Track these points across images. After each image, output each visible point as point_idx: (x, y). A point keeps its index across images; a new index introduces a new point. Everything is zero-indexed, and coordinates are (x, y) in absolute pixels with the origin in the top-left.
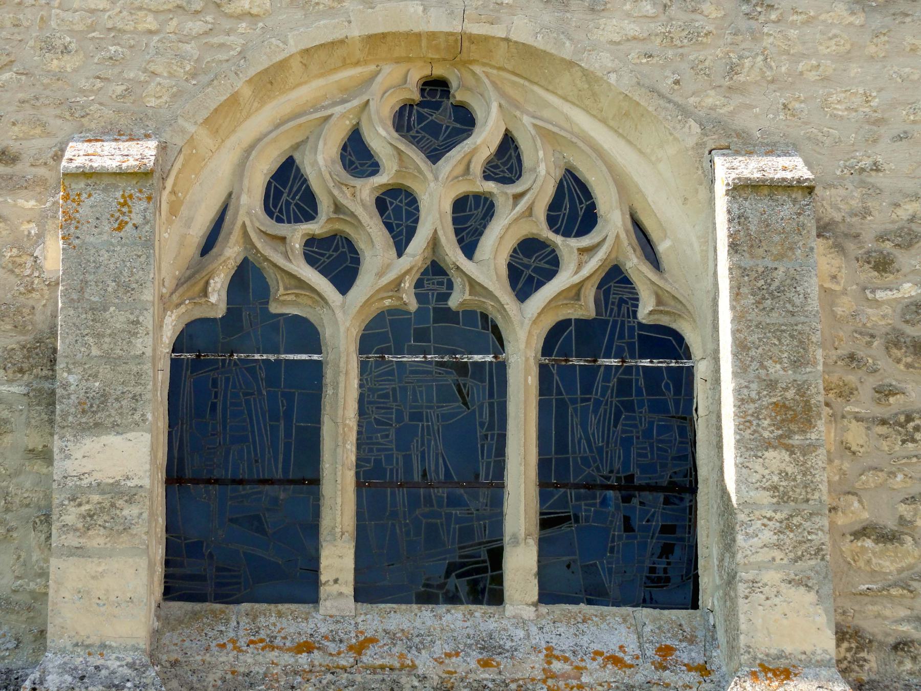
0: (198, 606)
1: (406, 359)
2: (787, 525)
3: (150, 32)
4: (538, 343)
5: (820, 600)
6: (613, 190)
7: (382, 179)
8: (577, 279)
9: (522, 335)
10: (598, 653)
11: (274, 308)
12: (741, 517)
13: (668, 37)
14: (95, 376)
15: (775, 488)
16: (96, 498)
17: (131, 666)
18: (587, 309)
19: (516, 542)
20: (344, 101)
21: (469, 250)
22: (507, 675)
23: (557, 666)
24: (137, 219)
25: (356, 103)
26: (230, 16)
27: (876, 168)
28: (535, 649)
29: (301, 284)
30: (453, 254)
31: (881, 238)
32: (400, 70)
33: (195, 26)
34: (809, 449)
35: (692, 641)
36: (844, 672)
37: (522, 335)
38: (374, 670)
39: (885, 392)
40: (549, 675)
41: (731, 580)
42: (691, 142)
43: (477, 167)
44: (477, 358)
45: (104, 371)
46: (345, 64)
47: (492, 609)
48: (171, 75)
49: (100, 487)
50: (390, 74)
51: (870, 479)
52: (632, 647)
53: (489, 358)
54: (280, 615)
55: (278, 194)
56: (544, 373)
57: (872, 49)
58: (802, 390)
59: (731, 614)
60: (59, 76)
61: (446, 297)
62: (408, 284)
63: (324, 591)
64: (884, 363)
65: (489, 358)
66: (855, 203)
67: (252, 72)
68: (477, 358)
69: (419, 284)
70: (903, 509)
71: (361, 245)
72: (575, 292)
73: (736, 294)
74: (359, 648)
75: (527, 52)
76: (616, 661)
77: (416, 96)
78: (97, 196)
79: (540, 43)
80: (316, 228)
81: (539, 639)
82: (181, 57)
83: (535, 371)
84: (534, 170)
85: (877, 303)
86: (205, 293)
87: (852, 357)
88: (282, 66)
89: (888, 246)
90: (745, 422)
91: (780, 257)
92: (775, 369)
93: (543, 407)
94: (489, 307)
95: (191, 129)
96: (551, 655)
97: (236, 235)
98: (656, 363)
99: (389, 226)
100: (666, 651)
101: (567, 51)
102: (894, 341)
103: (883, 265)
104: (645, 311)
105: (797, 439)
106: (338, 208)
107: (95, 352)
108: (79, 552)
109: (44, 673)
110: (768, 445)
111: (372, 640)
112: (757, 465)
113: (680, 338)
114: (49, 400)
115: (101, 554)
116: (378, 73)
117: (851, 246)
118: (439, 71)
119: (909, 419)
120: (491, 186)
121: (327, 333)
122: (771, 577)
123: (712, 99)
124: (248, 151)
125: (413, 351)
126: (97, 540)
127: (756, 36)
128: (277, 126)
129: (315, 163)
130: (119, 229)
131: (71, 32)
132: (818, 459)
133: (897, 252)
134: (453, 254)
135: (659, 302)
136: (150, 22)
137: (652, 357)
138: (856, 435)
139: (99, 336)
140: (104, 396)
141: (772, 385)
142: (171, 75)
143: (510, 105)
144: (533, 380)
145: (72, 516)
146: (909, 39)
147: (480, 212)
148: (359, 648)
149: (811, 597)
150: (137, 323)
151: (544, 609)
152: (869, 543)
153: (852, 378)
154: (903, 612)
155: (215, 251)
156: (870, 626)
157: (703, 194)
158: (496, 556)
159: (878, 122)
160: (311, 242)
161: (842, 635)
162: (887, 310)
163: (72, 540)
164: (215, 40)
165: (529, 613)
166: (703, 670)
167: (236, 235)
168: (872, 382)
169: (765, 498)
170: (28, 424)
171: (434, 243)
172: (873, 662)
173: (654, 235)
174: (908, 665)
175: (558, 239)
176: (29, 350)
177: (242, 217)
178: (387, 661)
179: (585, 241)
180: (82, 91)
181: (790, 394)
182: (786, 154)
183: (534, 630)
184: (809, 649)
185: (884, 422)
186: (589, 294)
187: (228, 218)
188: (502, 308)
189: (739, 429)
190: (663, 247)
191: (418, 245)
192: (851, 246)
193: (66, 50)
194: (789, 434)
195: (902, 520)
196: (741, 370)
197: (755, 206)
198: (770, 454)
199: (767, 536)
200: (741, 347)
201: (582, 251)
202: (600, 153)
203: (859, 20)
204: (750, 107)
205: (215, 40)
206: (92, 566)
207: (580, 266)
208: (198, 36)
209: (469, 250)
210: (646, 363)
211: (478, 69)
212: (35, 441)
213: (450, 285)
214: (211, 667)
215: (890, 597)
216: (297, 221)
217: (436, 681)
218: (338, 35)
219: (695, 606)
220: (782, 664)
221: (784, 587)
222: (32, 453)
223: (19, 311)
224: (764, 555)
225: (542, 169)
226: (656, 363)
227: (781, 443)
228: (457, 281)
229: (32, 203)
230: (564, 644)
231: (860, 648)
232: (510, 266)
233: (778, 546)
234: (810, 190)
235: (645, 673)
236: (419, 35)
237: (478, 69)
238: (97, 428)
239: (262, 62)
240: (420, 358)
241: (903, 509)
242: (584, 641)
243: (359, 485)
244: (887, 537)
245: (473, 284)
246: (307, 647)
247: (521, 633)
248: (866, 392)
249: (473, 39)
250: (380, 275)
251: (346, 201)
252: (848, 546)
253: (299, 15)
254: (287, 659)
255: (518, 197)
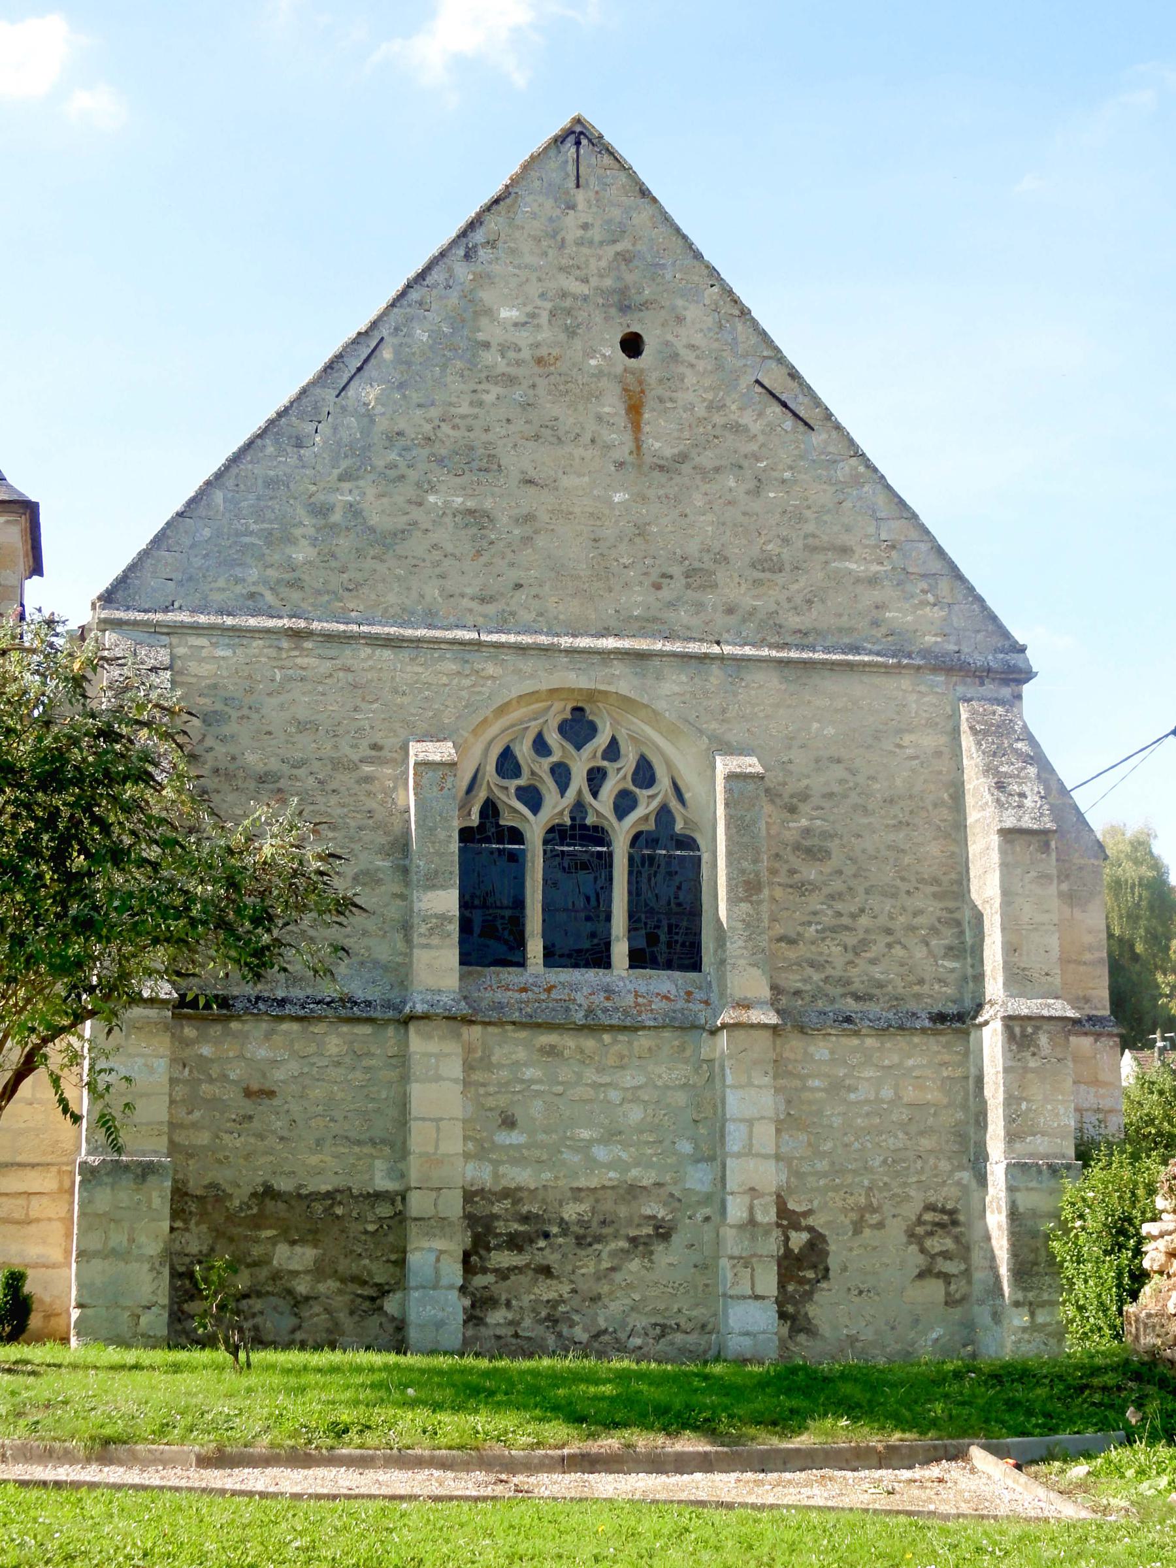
0: (470, 968)
1: (566, 849)
2: (749, 939)
3: (445, 685)
4: (628, 843)
5: (764, 973)
6: (664, 767)
7: (554, 759)
8: (647, 811)
9: (621, 838)
10: (658, 994)
11: (502, 822)
12: (729, 934)
13: (693, 694)
14: (432, 862)
15: (744, 921)
16: (434, 921)
17: (453, 1000)
18: (651, 826)
19: (618, 939)
20: (535, 719)
21: (595, 794)
22: (618, 1005)
23: (640, 1000)
24: (449, 785)
25: (541, 721)
26: (483, 677)
27: (790, 762)
28: (629, 991)
29: (515, 811)
30: (588, 797)
31: (792, 796)
32: (562, 703)
33: (466, 682)
34: (760, 902)
35: (700, 988)
36: (772, 1004)
37: (621, 838)
38: (557, 1001)
39: (792, 872)
40: (637, 1004)
41: (723, 962)
42: (704, 747)
43: (599, 754)
44: (599, 849)
45: (436, 859)
46: (537, 701)
47: (606, 971)
48: (455, 707)
49: (436, 916)
50: (558, 706)
51: (785, 914)
52: (674, 992)
53: (605, 849)
54: (509, 973)
55: (503, 765)
56: (631, 859)
57: (789, 702)
58: (757, 874)
59: (722, 979)
60: (401, 707)
61: (584, 818)
62: (566, 812)
63: (529, 962)
64: (792, 858)
65: (605, 849)
66: (780, 779)
67: (495, 707)
68: (599, 849)
69: (571, 812)
70: (800, 929)
71: (544, 791)
72: (646, 818)
73: (728, 827)
74: (549, 990)
75: (626, 699)
76: (667, 998)
77: (570, 717)
78: (430, 774)
79: (632, 695)
80: (521, 782)
81: (630, 987)
82: (460, 699)
83: (626, 856)
84: (627, 756)
85: (789, 829)
86: (469, 814)
87: (777, 855)
88: (508, 703)
89: (795, 800)
90: (731, 889)
91: (748, 810)
92: (745, 864)
93: (630, 873)
94: (605, 824)
95: (466, 734)
96: (637, 996)
97: (484, 786)
98: (683, 853)
99: (556, 782)
100: (689, 993)
101: (645, 700)
102: (797, 847)
103: (792, 810)
104: (679, 827)
105: (754, 898)
106: (533, 773)
107: (432, 850)
108: (427, 946)
109: (414, 1003)
110: (742, 900)
111: (554, 987)
112: (736, 909)
113: (694, 841)
114: (405, 871)
115: (437, 947)
116: (551, 706)
117: (778, 801)
118: (580, 705)
119: (803, 885)
120: (605, 763)
121: (528, 835)
122: (742, 962)
123: (714, 725)
124: (490, 743)
125: (569, 845)
126: (435, 941)
127: (735, 694)
128: (503, 732)
129: (521, 750)
130: (441, 790)
131: (406, 684)
132: (765, 907)
133: (799, 804)
134: (588, 797)
135: (686, 823)
136: (445, 680)
137: (682, 850)
138: (779, 893)
139: (434, 843)
140: (436, 872)
141: (743, 872)
142: (455, 707)
143: (615, 723)
144: (626, 861)
145: (423, 929)
146: (808, 698)
147: (600, 776)
148: (549, 990)
149: (760, 972)
150: (450, 836)
151: (631, 971)
152: (783, 944)
153: (777, 865)
154: (799, 977)
155: (474, 793)
156: (782, 983)
157: (709, 773)
158: (608, 945)
159: (792, 739)
160: (519, 789)
161: (772, 988)
162: (794, 832)
163: (424, 941)
164: (477, 689)
165: (624, 974)
166: (707, 1003)
167: (484, 786)
168: (786, 867)
169: (740, 925)
170: (393, 881)
171: (580, 792)
172: (784, 1001)
173: (683, 790)
174: (800, 1002)
175: (637, 790)
176: (393, 844)
177: (487, 778)
178: (562, 997)
179: (650, 792)
180: (413, 715)
181: (752, 876)
182: (749, 755)
183: (627, 982)
184: (757, 995)
185: (791, 887)
186: (652, 818)
187: (479, 776)
188: (611, 825)
189: (728, 892)
190: (687, 796)
191: (571, 793)
192: (778, 801)
193: (404, 694)
194: (751, 896)
195: (799, 934)
196: (729, 864)
197: (737, 785)
198: (742, 904)
199: (741, 943)
200: (729, 854)
201: (649, 797)
202: (658, 748)
203: (783, 687)
204: (731, 730)
205: (477, 689)
206: (434, 953)
207: (648, 805)
208: (468, 687)
209: (595, 794)
210: (678, 853)
211: (600, 705)
212: (397, 889)
213: (586, 813)
214: (482, 999)
215: (792, 970)
216: (512, 778)
217: (586, 1007)
218: (536, 688)
219: (700, 971)
220: (746, 1003)
221: (748, 968)
222: (395, 896)
223: (386, 825)
224: (739, 952)
225: (631, 756)
226: (683, 853)
227: (747, 899)
228: (590, 811)
229: (390, 771)
230: (642, 990)
231: (778, 994)
232: (614, 803)
233: (745, 948)
234: (763, 778)
235: (680, 1004)
236: (574, 690)
237: (600, 705)
238: (433, 887)
239: (499, 702)
240: (571, 848)
241: (800, 929)
242: (651, 988)
243: (543, 910)
244: (792, 942)
245: (598, 813)
246: (524, 990)
247: (621, 984)
248: (783, 871)
249: (600, 692)
250: (554, 807)
251: (537, 770)
252: (774, 946)
253: (516, 678)
254: (517, 995)
255: (619, 770)
